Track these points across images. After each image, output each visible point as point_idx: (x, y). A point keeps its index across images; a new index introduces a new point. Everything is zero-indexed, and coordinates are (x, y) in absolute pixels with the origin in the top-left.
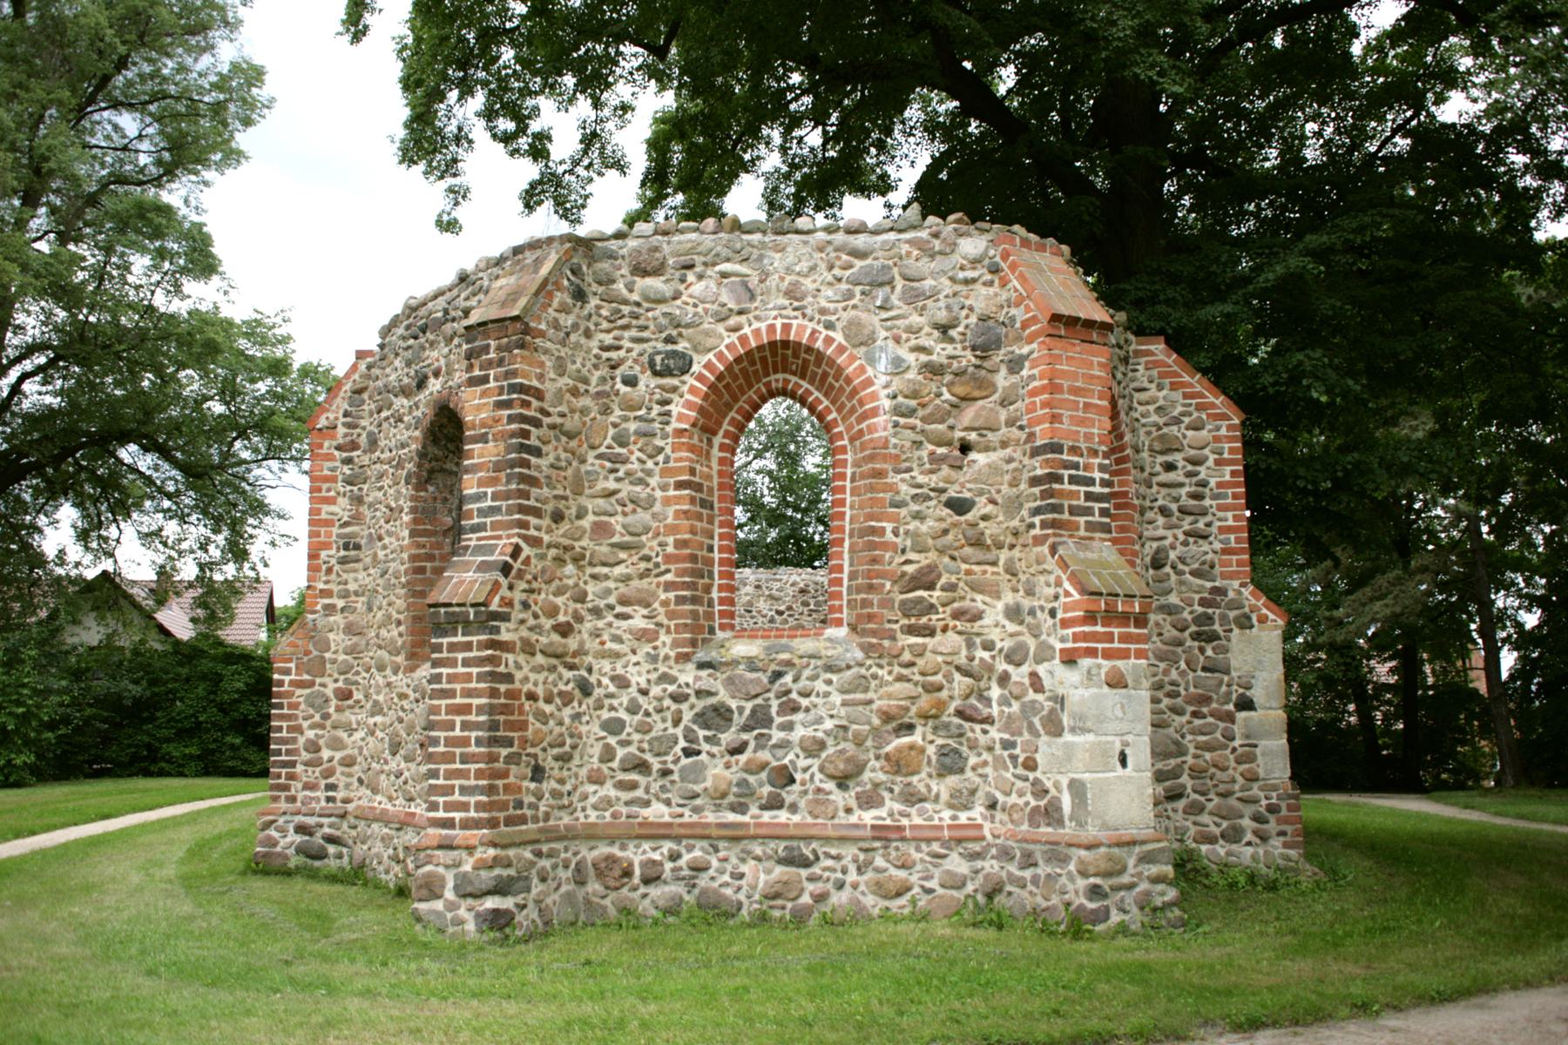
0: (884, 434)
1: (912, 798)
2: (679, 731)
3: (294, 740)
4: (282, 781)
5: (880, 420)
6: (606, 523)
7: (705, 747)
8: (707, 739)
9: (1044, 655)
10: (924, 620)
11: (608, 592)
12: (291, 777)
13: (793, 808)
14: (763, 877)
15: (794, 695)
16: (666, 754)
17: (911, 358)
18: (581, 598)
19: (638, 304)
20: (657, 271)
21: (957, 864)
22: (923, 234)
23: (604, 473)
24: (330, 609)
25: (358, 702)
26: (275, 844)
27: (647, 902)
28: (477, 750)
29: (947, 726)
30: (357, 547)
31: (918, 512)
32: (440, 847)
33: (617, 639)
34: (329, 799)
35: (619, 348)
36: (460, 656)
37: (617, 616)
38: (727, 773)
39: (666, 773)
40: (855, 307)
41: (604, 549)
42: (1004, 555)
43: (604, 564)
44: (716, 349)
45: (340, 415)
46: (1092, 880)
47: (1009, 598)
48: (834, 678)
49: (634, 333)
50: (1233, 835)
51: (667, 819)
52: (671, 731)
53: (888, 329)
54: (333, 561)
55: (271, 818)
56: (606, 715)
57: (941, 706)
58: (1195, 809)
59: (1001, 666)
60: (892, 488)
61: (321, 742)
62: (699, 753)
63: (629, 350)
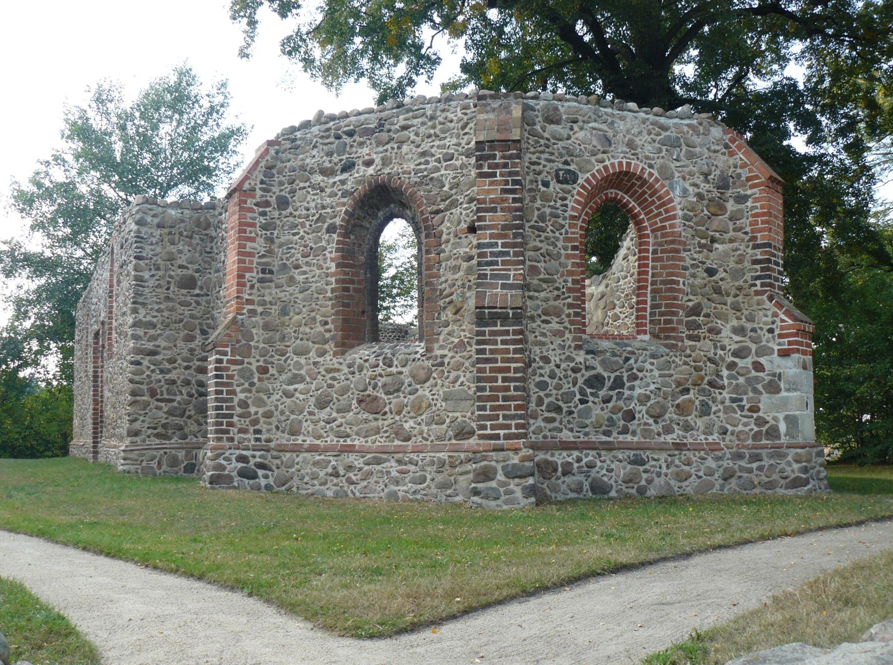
0: (679, 229)
2: (576, 389)
3: (231, 400)
4: (224, 427)
5: (677, 221)
6: (537, 267)
7: (591, 398)
8: (592, 394)
9: (764, 351)
10: (696, 332)
11: (538, 307)
12: (230, 424)
13: (634, 433)
14: (622, 472)
15: (635, 371)
16: (570, 402)
17: (691, 189)
19: (548, 140)
20: (558, 122)
21: (711, 463)
22: (695, 122)
23: (534, 236)
24: (253, 313)
25: (273, 375)
26: (224, 468)
27: (565, 485)
28: (516, 393)
29: (704, 390)
30: (271, 272)
31: (694, 274)
32: (494, 450)
33: (544, 335)
34: (257, 440)
35: (539, 164)
36: (499, 339)
37: (544, 322)
38: (602, 413)
39: (571, 413)
40: (663, 157)
41: (535, 282)
42: (730, 300)
43: (535, 291)
45: (258, 182)
46: (804, 464)
47: (735, 323)
48: (655, 361)
49: (546, 156)
51: (572, 439)
52: (572, 389)
53: (679, 172)
54: (255, 281)
55: (221, 451)
56: (538, 379)
60: (682, 259)
61: (249, 401)
62: (587, 402)
63: (545, 166)
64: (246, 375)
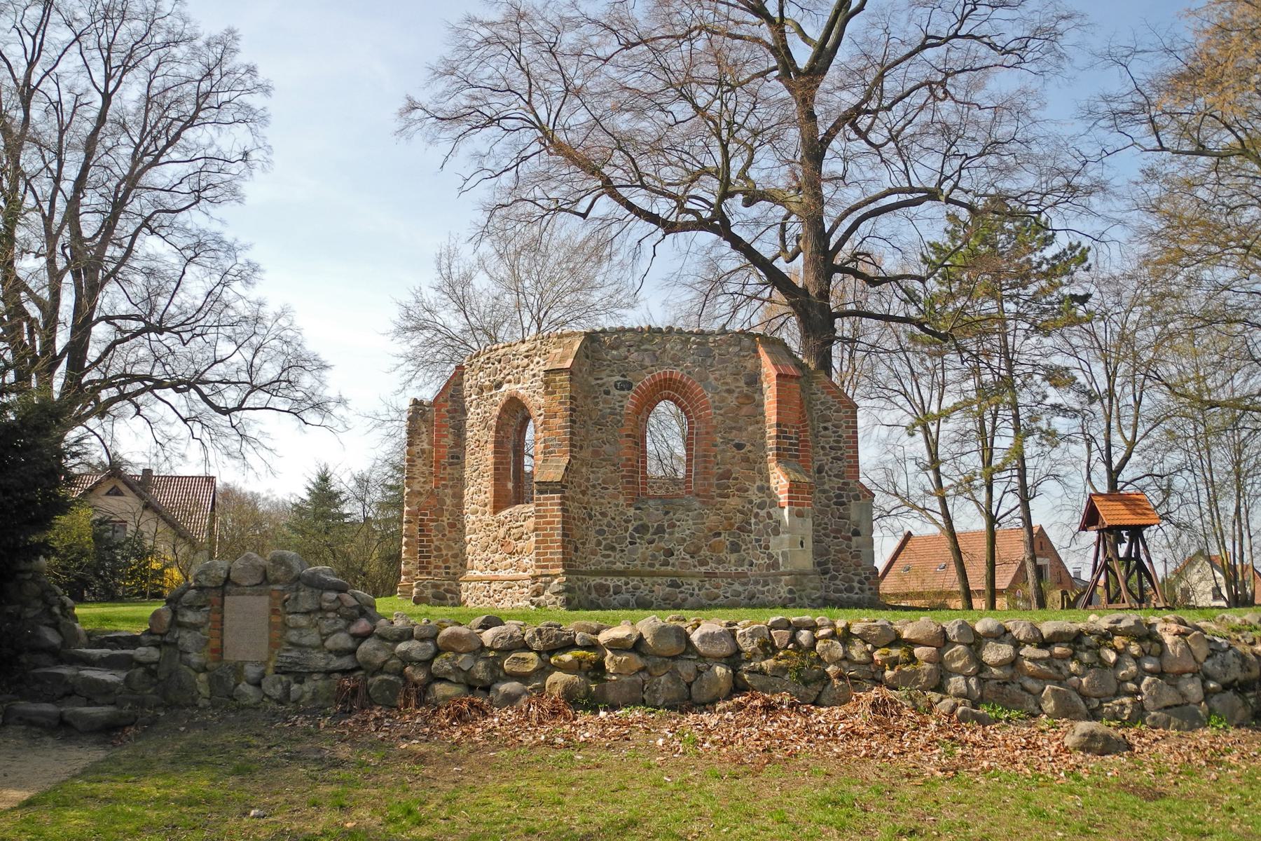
1: (720, 562)
18: (588, 480)
21: (737, 587)
24: (445, 486)
39: (623, 551)
44: (645, 380)
47: (758, 483)
50: (850, 589)
57: (732, 525)
58: (834, 578)
59: (756, 510)
64: (440, 529)
